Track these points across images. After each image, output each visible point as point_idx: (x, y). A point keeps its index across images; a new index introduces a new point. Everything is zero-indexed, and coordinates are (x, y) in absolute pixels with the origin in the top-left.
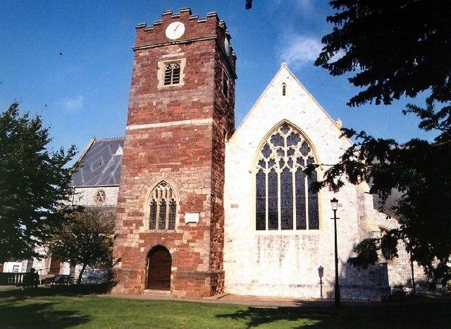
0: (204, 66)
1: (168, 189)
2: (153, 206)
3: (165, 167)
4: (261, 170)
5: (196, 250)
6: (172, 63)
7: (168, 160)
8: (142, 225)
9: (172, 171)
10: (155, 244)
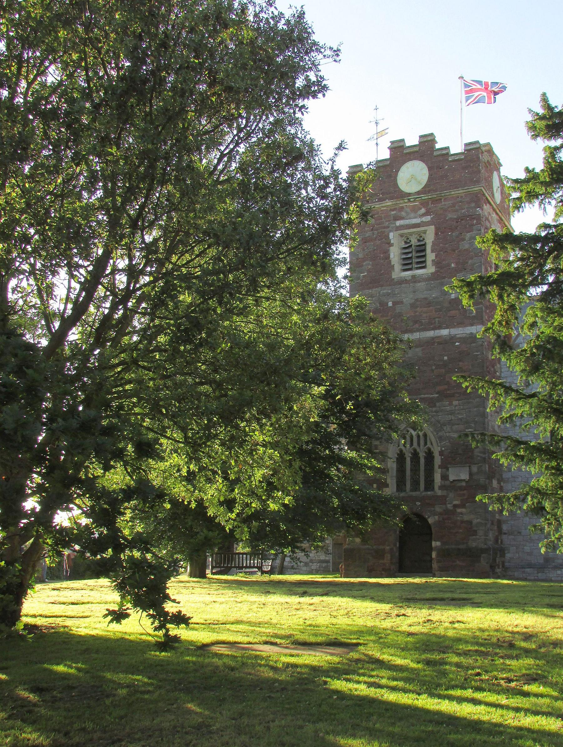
0: (463, 240)
1: (421, 434)
2: (401, 458)
5: (466, 518)
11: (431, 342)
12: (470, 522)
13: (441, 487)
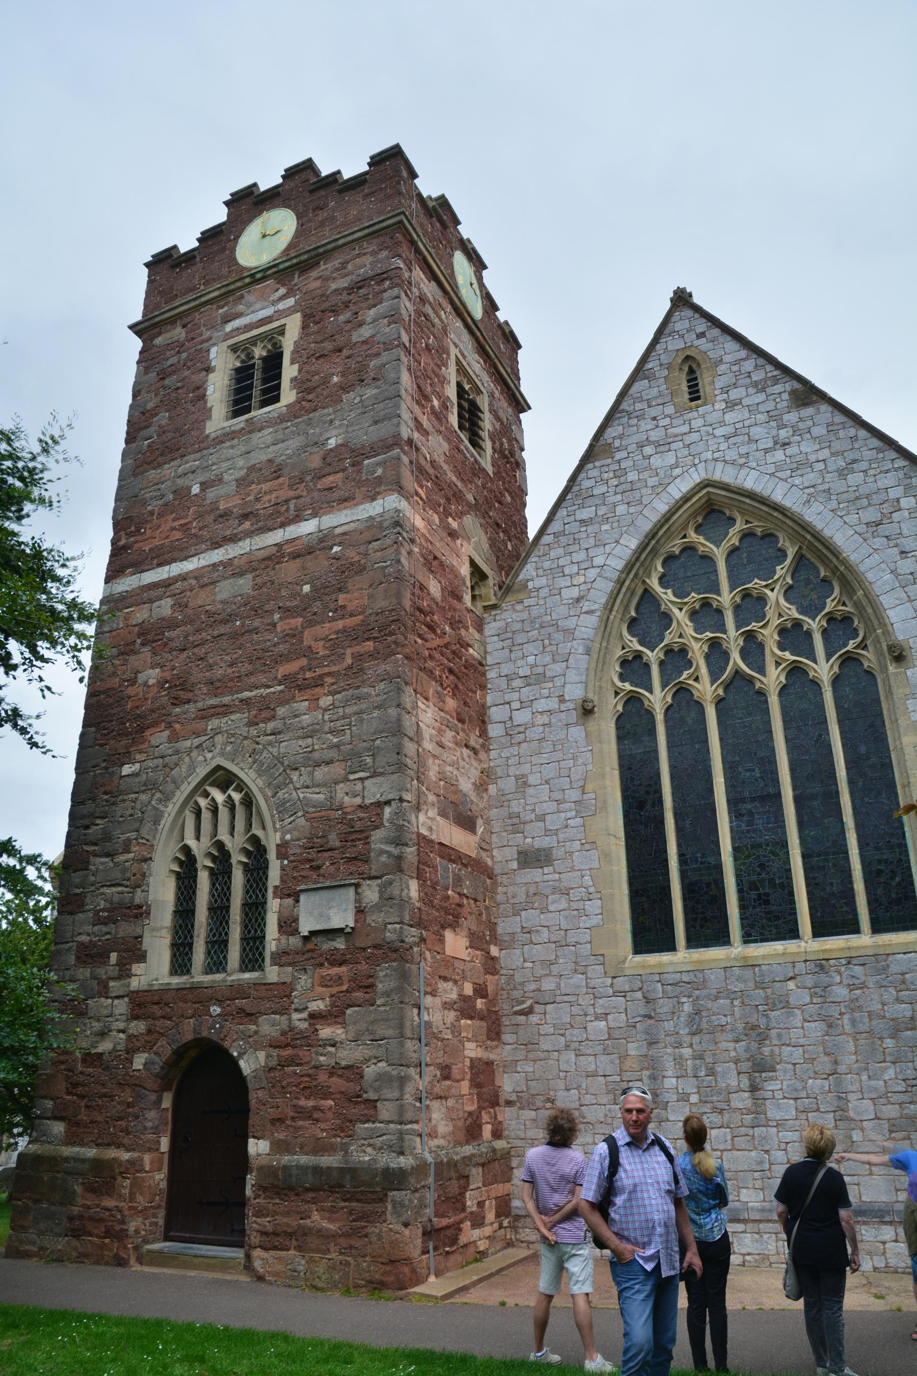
2: (187, 862)
3: (224, 710)
4: (633, 700)
5: (346, 1056)
6: (253, 341)
8: (142, 957)
9: (252, 723)
10: (188, 1031)
12: (353, 1072)
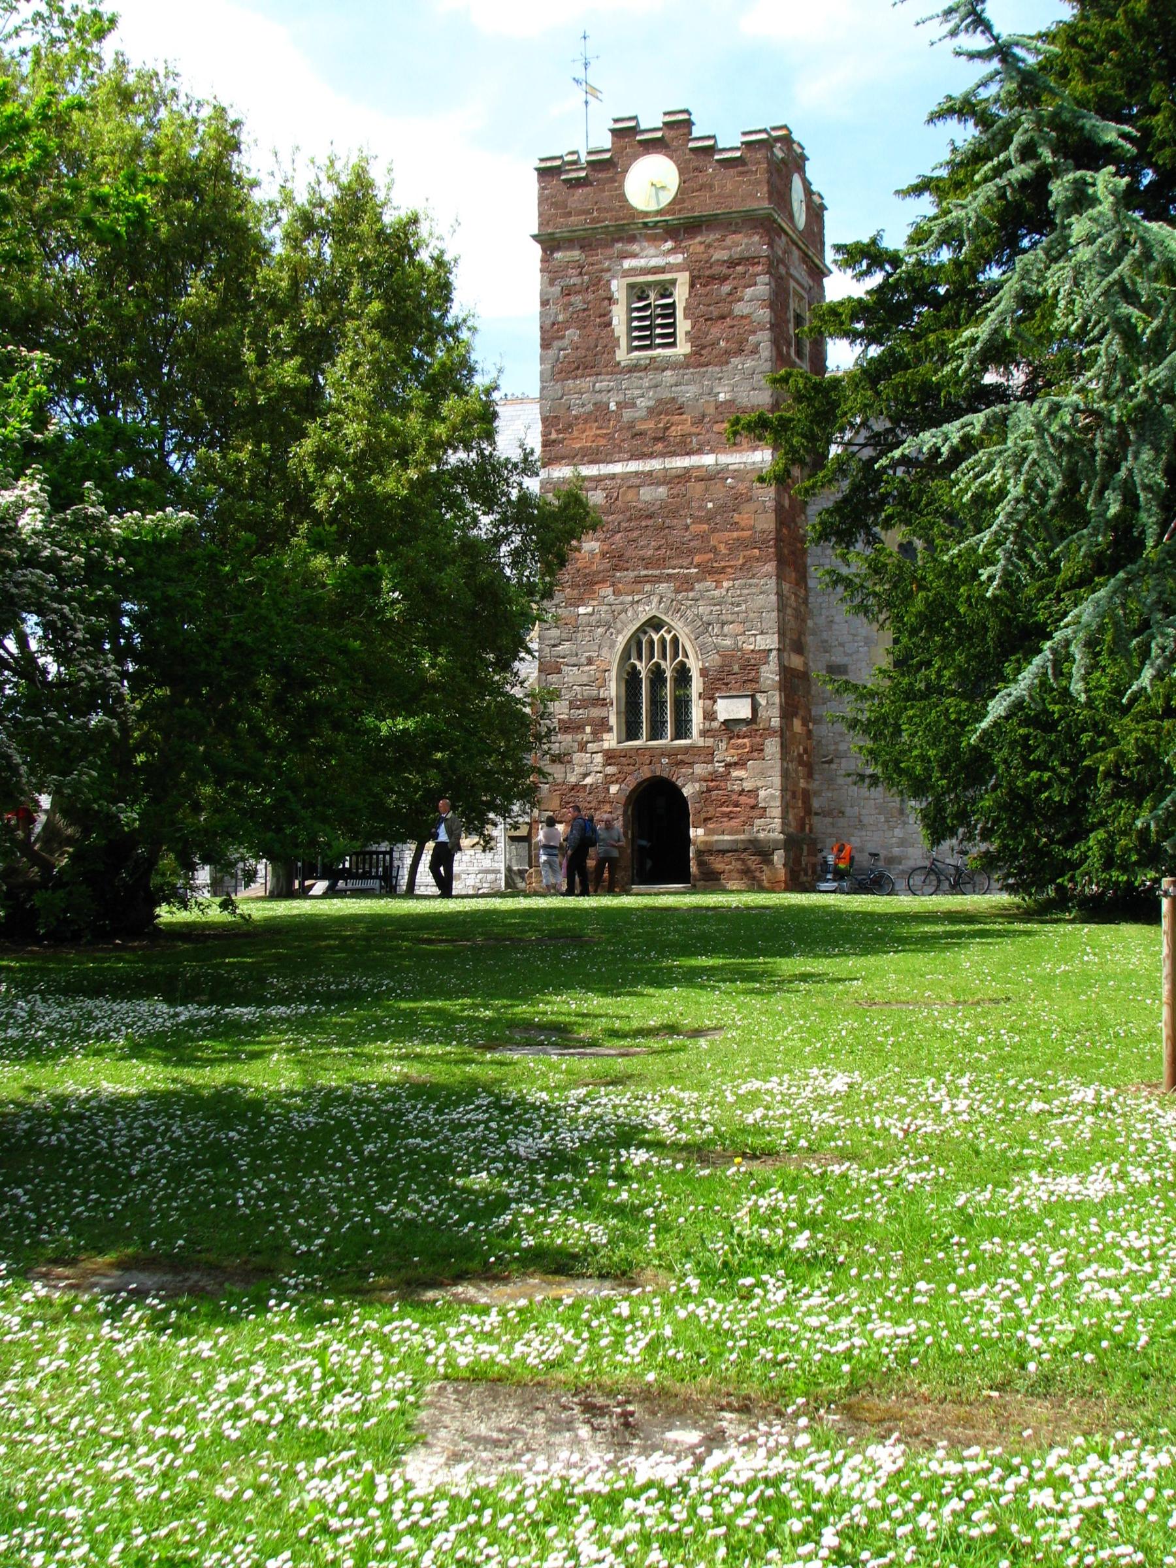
1: (668, 637)
2: (631, 680)
3: (657, 580)
5: (747, 786)
7: (660, 563)
10: (646, 773)
11: (685, 476)
12: (754, 792)
13: (704, 733)
